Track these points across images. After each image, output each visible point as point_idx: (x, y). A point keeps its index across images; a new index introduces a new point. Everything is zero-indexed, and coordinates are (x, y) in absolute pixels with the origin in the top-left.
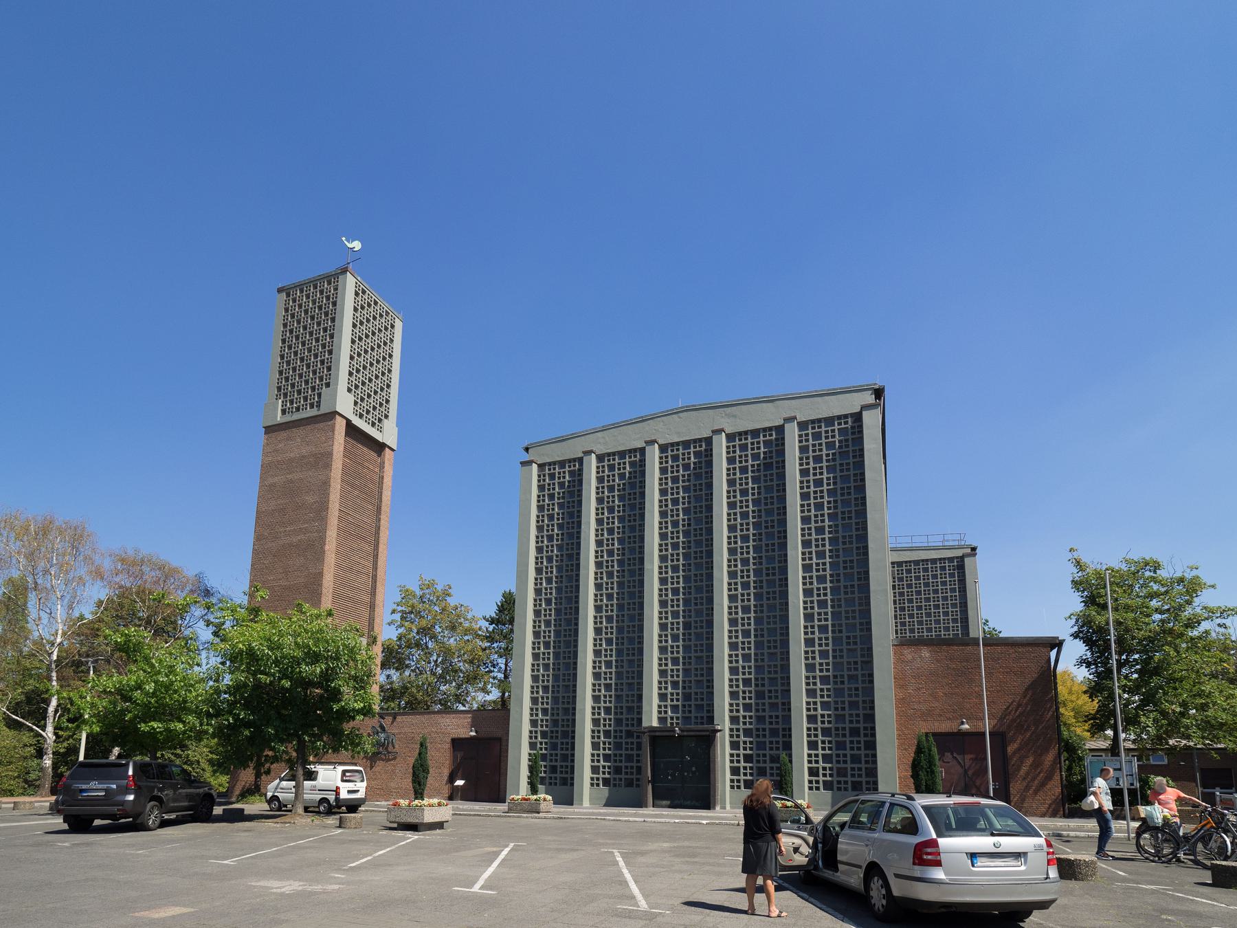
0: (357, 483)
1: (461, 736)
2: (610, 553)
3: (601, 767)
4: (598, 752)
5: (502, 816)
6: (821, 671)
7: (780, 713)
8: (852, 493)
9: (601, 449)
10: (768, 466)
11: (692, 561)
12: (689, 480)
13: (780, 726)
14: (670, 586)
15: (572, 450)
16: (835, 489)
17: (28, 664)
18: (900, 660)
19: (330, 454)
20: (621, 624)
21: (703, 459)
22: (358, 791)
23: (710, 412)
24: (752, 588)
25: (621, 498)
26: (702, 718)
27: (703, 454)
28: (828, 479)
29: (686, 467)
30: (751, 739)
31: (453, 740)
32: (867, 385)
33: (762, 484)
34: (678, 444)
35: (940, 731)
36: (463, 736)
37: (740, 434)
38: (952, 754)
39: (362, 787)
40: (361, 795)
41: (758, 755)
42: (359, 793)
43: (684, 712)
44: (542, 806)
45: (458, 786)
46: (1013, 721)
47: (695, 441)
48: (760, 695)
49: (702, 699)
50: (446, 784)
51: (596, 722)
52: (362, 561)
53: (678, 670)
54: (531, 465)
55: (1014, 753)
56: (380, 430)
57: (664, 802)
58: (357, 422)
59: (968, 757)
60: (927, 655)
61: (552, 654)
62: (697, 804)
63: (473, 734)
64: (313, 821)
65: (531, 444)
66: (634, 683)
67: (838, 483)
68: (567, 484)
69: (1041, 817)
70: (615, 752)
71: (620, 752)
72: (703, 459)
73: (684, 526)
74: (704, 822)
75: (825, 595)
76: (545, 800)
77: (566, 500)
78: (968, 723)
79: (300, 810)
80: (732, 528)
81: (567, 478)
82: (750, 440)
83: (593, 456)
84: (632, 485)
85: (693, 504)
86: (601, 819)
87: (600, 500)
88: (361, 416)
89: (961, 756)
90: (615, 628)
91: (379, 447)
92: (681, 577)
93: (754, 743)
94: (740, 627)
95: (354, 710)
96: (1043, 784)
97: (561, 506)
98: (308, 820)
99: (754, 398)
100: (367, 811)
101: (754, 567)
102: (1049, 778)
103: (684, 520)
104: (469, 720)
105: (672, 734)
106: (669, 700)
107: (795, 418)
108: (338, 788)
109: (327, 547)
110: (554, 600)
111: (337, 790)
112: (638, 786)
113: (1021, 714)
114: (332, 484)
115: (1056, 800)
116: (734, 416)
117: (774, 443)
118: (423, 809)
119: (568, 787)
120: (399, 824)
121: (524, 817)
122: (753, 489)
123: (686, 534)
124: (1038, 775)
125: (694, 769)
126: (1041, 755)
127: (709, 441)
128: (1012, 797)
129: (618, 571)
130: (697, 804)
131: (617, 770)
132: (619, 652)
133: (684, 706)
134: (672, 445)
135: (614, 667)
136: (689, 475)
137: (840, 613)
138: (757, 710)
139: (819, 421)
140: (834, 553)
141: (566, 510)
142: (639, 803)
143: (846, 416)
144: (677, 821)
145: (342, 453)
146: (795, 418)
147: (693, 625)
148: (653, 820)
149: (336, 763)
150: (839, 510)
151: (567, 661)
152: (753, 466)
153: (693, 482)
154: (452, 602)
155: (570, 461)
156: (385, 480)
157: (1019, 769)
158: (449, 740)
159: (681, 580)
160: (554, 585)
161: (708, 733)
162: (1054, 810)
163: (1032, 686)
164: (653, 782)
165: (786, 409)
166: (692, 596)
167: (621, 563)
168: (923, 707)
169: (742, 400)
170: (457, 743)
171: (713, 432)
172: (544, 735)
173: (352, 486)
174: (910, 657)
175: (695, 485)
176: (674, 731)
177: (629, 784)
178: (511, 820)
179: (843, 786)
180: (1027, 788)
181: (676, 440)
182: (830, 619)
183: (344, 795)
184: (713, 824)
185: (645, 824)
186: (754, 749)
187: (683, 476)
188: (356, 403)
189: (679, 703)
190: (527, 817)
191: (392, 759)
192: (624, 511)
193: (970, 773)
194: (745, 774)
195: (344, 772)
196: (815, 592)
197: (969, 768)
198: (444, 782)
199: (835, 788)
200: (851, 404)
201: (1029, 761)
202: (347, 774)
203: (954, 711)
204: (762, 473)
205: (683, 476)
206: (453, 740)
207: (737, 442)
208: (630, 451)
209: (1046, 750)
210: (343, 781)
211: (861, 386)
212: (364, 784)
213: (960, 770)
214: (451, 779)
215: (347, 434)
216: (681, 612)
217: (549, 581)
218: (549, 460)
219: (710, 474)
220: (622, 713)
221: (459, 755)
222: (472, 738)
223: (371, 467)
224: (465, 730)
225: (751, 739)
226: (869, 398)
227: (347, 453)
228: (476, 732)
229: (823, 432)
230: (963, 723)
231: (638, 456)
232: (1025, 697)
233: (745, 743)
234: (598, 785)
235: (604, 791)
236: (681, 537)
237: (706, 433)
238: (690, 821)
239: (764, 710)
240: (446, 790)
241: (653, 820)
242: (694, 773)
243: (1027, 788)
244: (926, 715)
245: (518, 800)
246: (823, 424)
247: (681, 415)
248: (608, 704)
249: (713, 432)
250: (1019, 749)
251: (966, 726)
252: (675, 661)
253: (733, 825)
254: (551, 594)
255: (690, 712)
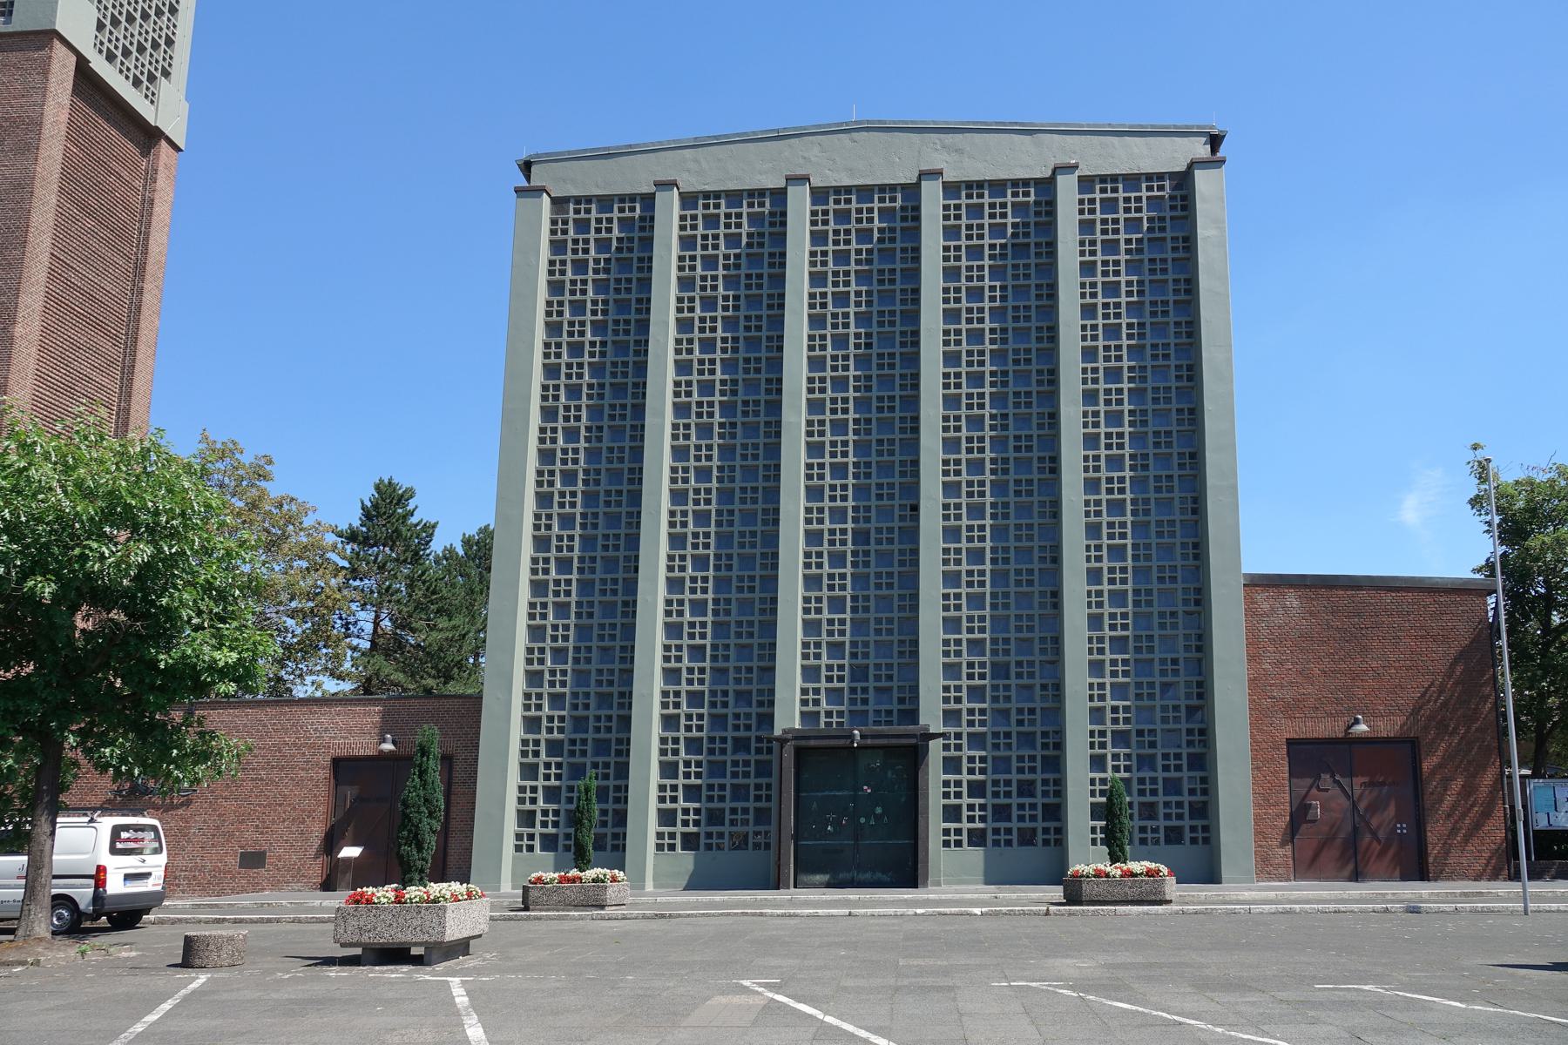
0: (92, 202)
1: (356, 753)
2: (706, 388)
3: (679, 813)
4: (674, 782)
5: (510, 919)
6: (1113, 627)
7: (615, 712)
8: (898, 323)
9: (690, 183)
10: (1020, 249)
11: (606, 423)
12: (869, 262)
13: (613, 736)
14: (692, 463)
15: (634, 178)
16: (1140, 303)
17: (305, 540)
18: (1251, 612)
19: (37, 124)
20: (725, 528)
21: (636, 234)
22: (147, 875)
23: (914, 137)
24: (988, 472)
25: (730, 282)
26: (889, 713)
27: (637, 224)
28: (1129, 283)
29: (733, 240)
30: (983, 753)
31: (337, 762)
32: (1198, 127)
33: (1010, 282)
34: (848, 190)
35: (1315, 735)
36: (362, 753)
37: (969, 185)
38: (1333, 776)
39: (156, 864)
40: (153, 885)
41: (995, 783)
42: (151, 881)
43: (853, 701)
44: (610, 891)
45: (347, 860)
46: (1430, 718)
47: (882, 188)
48: (1000, 670)
49: (890, 678)
50: (316, 857)
51: (669, 722)
52: (94, 375)
53: (842, 622)
54: (540, 196)
55: (1433, 772)
56: (152, 98)
57: (818, 878)
58: (99, 65)
59: (1358, 781)
60: (1296, 603)
61: (574, 583)
62: (885, 878)
63: (388, 747)
64: (83, 953)
65: (537, 155)
66: (613, 648)
67: (1010, 298)
68: (614, 243)
69: (1475, 880)
70: (711, 781)
71: (721, 781)
72: (636, 234)
73: (857, 346)
74: (977, 911)
75: (708, 502)
76: (614, 880)
77: (612, 276)
78: (1365, 722)
79: (42, 923)
80: (683, 367)
81: (616, 232)
82: (723, 209)
83: (546, 199)
84: (624, 264)
85: (875, 308)
86: (754, 915)
87: (685, 283)
88: (110, 57)
89: (1348, 780)
90: (713, 535)
91: (148, 136)
92: (716, 448)
93: (990, 760)
94: (689, 551)
95: (212, 667)
96: (1477, 826)
97: (600, 286)
98: (67, 952)
99: (997, 123)
100: (161, 922)
101: (721, 441)
102: (1486, 814)
103: (857, 336)
104: (377, 719)
105: (841, 742)
106: (684, 682)
107: (940, 173)
108: (101, 870)
109: (18, 330)
110: (715, 473)
111: (99, 877)
112: (615, 848)
113: (1445, 704)
114: (38, 191)
115: (1497, 850)
116: (959, 151)
117: (1032, 209)
118: (444, 909)
119: (620, 853)
120: (367, 948)
121: (573, 918)
122: (992, 288)
123: (862, 362)
124: (1469, 810)
125: (879, 810)
126: (1474, 776)
127: (648, 200)
128: (1430, 847)
129: (721, 425)
130: (885, 878)
131: (715, 817)
132: (721, 584)
133: (853, 690)
134: (838, 190)
135: (710, 612)
136: (607, 261)
137: (595, 538)
138: (995, 699)
139: (1114, 178)
140: (728, 430)
141: (612, 296)
142: (774, 882)
143: (1160, 176)
144: (919, 911)
145: (63, 127)
146: (1215, 163)
147: (873, 535)
148: (870, 911)
149: (94, 810)
150: (609, 359)
151: (609, 598)
152: (726, 257)
153: (876, 266)
154: (274, 489)
155: (622, 198)
156: (156, 209)
157: (1441, 801)
158: (326, 761)
159: (715, 452)
160: (716, 440)
161: (913, 741)
162: (1494, 868)
163: (1463, 655)
164: (797, 837)
165: (663, 167)
166: (602, 488)
167: (727, 408)
168: (1288, 694)
169: (974, 123)
170: (343, 768)
171: (788, 179)
172: (554, 748)
173: (83, 207)
174: (1266, 606)
175: (881, 272)
176: (852, 737)
177: (1027, 839)
178: (566, 925)
179: (1002, 837)
180: (1454, 831)
181: (847, 182)
182: (1129, 535)
183: (115, 886)
184: (997, 914)
185: (852, 920)
186: (564, 777)
187: (859, 252)
188: (100, 26)
189: (566, 690)
190: (581, 918)
191: (182, 805)
192: (1004, 298)
193: (1362, 806)
194: (971, 819)
195: (116, 831)
196: (827, 492)
197: (1360, 798)
198: (312, 852)
199: (702, 847)
200: (1171, 156)
201: (1457, 785)
202: (124, 835)
203: (1338, 702)
204: (1010, 262)
205: (859, 252)
206: (337, 762)
207: (831, 206)
208: (751, 193)
209: (1483, 767)
210: (114, 851)
211: (1187, 127)
212: (162, 859)
213: (1346, 803)
214: (331, 843)
215: (77, 91)
216: (850, 511)
217: (571, 435)
218: (575, 193)
219: (646, 264)
220: (725, 705)
221: (350, 793)
222: (383, 757)
223: (125, 174)
224: (366, 740)
225: (983, 753)
226: (1202, 150)
227: (75, 132)
228: (394, 743)
229: (854, 212)
230: (1357, 722)
231: (768, 204)
232: (1450, 677)
233: (971, 759)
234: (531, 848)
235: (686, 860)
236: (852, 367)
237: (907, 176)
238: (947, 910)
239: (725, 705)
240: (316, 870)
241: (870, 911)
242: (878, 818)
243: (1454, 831)
244: (1291, 709)
245: (552, 880)
246: (854, 198)
247: (855, 135)
248: (696, 687)
249: (788, 179)
250: (1441, 766)
251: (1363, 727)
252: (837, 604)
253: (1036, 914)
254: (575, 461)
255: (865, 701)
